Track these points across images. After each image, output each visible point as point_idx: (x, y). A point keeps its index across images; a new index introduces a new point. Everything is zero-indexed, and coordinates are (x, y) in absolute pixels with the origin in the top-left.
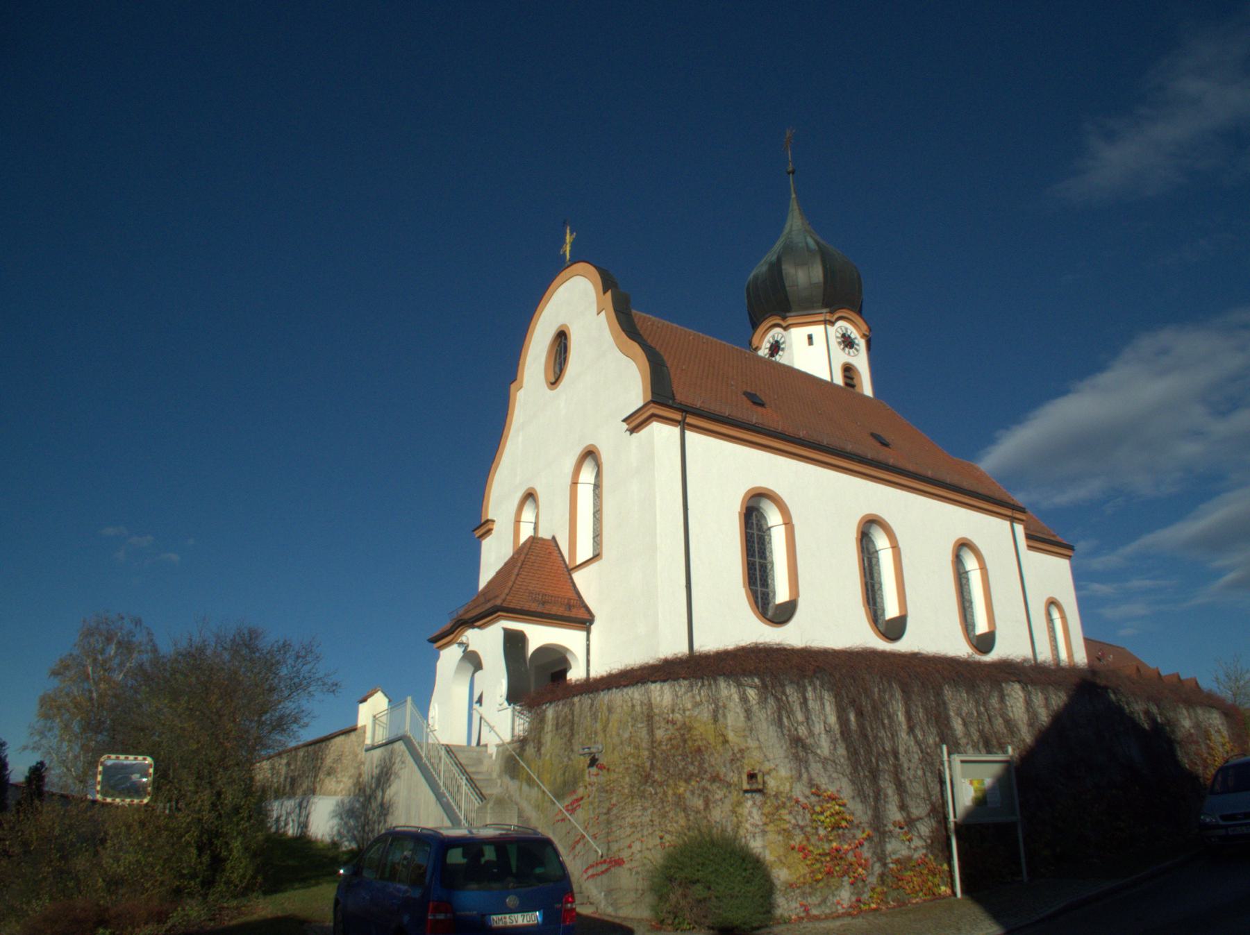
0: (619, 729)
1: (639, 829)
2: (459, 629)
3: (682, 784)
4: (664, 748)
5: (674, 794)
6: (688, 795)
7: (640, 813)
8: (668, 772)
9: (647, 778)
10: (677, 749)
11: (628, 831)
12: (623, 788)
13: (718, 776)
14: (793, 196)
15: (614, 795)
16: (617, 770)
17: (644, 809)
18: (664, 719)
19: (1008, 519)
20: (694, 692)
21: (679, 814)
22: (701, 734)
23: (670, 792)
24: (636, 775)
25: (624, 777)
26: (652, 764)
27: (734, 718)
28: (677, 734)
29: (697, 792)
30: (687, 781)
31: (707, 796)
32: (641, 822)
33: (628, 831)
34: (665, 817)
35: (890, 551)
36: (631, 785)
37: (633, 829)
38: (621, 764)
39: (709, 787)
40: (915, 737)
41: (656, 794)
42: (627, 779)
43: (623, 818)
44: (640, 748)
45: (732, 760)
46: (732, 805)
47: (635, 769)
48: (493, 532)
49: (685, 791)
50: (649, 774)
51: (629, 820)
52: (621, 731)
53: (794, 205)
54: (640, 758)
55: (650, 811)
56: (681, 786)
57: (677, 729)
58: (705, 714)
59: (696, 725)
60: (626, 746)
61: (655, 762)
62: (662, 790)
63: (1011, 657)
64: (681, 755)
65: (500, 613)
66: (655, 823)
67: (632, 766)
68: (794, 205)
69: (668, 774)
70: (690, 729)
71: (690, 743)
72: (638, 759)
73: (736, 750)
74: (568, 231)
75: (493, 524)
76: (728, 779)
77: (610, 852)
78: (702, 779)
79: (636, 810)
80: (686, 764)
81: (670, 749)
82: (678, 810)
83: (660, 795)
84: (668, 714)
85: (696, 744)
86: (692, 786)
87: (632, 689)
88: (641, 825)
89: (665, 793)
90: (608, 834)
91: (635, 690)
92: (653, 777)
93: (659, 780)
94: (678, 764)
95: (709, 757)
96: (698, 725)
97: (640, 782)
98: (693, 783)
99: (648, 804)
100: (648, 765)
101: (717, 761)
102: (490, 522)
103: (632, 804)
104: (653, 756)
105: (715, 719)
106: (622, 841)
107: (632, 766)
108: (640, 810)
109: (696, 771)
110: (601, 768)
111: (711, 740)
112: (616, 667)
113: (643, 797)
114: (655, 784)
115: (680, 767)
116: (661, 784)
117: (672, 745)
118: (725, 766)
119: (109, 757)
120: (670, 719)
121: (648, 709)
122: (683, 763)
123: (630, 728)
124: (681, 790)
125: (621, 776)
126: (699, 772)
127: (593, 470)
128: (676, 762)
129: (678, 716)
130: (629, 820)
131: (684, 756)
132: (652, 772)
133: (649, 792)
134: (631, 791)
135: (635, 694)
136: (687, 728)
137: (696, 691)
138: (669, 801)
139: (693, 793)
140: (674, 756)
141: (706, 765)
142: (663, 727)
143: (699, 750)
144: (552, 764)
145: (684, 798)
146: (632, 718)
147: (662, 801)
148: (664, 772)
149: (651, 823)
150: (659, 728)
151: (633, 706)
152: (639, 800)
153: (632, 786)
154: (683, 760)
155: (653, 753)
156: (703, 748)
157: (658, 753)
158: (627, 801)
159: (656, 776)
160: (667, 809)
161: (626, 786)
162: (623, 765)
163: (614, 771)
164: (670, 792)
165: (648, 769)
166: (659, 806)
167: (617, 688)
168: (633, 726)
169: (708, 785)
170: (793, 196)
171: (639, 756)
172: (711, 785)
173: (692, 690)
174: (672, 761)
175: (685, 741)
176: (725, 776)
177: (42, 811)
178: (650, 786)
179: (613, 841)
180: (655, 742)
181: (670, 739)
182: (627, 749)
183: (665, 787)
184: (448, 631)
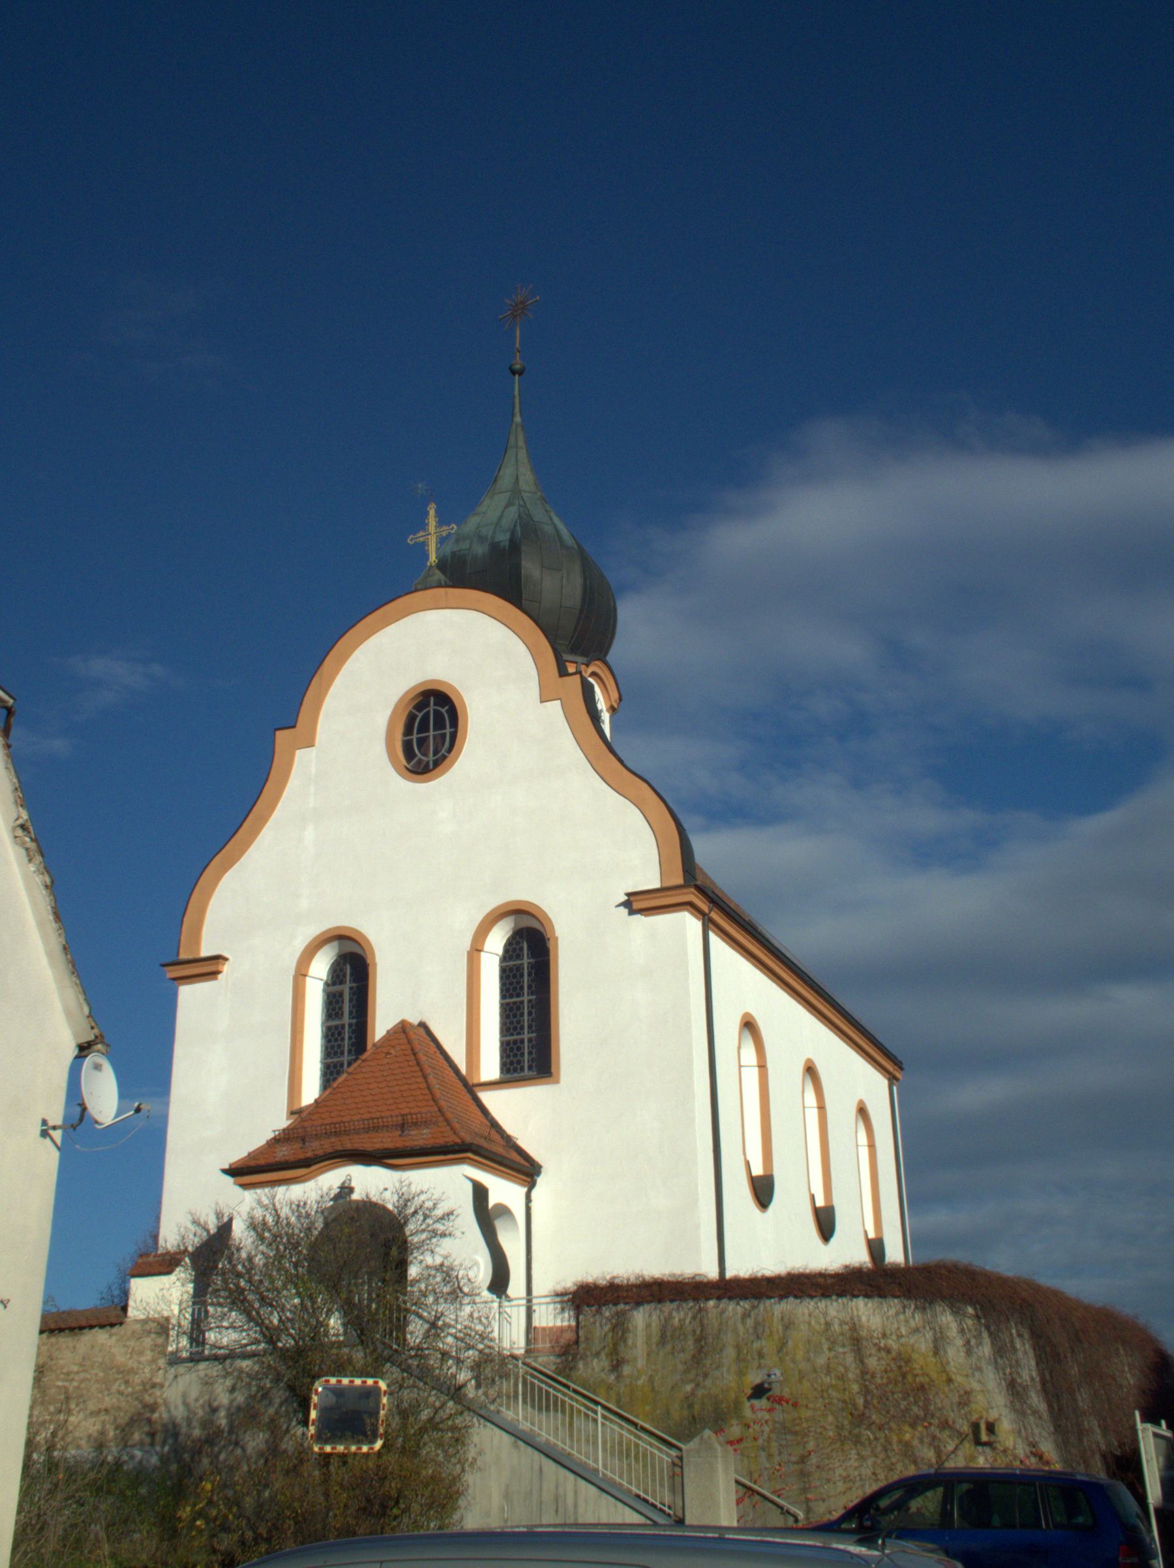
0: (808, 1351)
1: (858, 1484)
2: (328, 1162)
3: (907, 1428)
4: (879, 1381)
5: (900, 1441)
6: (916, 1442)
7: (856, 1464)
8: (888, 1412)
9: (859, 1419)
10: (896, 1384)
11: (841, 1486)
12: (825, 1428)
13: (947, 1422)
14: (518, 419)
15: (811, 1438)
16: (811, 1405)
17: (862, 1458)
18: (876, 1345)
19: (887, 1075)
20: (907, 1314)
21: (909, 1467)
22: (922, 1368)
23: (895, 1439)
24: (844, 1414)
25: (824, 1416)
26: (866, 1401)
27: (955, 1354)
28: (893, 1366)
29: (926, 1440)
30: (913, 1426)
31: (938, 1446)
32: (860, 1475)
33: (841, 1486)
34: (892, 1470)
35: (816, 1111)
36: (837, 1427)
37: (850, 1484)
38: (816, 1398)
39: (938, 1435)
40: (288, 1427)
41: (876, 1439)
42: (830, 1418)
43: (830, 1469)
44: (845, 1379)
45: (960, 1403)
46: (965, 1459)
47: (840, 1405)
48: (220, 976)
49: (913, 1438)
50: (863, 1414)
51: (839, 1471)
52: (812, 1355)
53: (519, 439)
54: (847, 1393)
55: (870, 1461)
56: (906, 1432)
57: (893, 1359)
58: (923, 1343)
59: (915, 1356)
60: (822, 1375)
61: (869, 1398)
62: (883, 1435)
63: (590, 1280)
64: (901, 1392)
65: (470, 1155)
66: (879, 1476)
67: (835, 1401)
68: (519, 439)
69: (888, 1416)
70: (908, 1361)
71: (909, 1377)
72: (844, 1394)
73: (962, 1392)
74: (432, 513)
75: (224, 964)
76: (958, 1426)
77: (811, 1515)
78: (930, 1424)
79: (850, 1458)
80: (908, 1404)
81: (887, 1384)
82: (907, 1461)
83: (882, 1441)
84: (878, 1338)
85: (918, 1379)
86: (919, 1432)
87: (823, 1302)
88: (861, 1479)
89: (887, 1439)
90: (804, 1490)
91: (829, 1304)
92: (869, 1417)
93: (878, 1421)
94: (899, 1404)
95: (934, 1397)
96: (917, 1356)
97: (851, 1423)
98: (920, 1429)
99: (866, 1452)
100: (860, 1401)
101: (943, 1401)
102: (221, 961)
103: (842, 1450)
104: (866, 1391)
105: (936, 1352)
106: (832, 1499)
107: (835, 1401)
108: (856, 1460)
109: (921, 1413)
110: (780, 1400)
111: (934, 1375)
112: (772, 1268)
113: (857, 1441)
114: (873, 1427)
115: (902, 1407)
116: (880, 1428)
117: (888, 1378)
118: (953, 1411)
119: (412, 1333)
120: (882, 1345)
121: (850, 1329)
122: (905, 1403)
123: (827, 1352)
124: (907, 1437)
125: (819, 1413)
126: (925, 1415)
127: (507, 933)
128: (897, 1401)
129: (892, 1343)
130: (839, 1471)
131: (906, 1395)
132: (867, 1412)
133: (865, 1437)
134: (840, 1435)
135: (834, 1309)
136: (903, 1360)
137: (908, 1312)
138: (894, 1450)
139: (921, 1441)
140: (893, 1393)
141: (932, 1407)
142: (875, 1356)
143: (922, 1388)
144: (653, 1390)
145: (912, 1447)
146: (827, 1339)
147: (885, 1449)
148: (884, 1412)
149: (874, 1477)
150: (870, 1355)
151: (828, 1324)
152: (853, 1446)
153: (840, 1428)
154: (904, 1399)
155: (866, 1387)
156: (927, 1386)
157: (872, 1387)
158: (834, 1446)
159: (874, 1417)
160: (893, 1460)
161: (829, 1427)
162: (821, 1400)
163: (806, 1406)
164: (895, 1439)
165: (861, 1407)
166: (882, 1456)
167: (796, 1297)
168: (830, 1349)
169: (937, 1432)
170: (518, 419)
171: (845, 1390)
172: (940, 1432)
173: (904, 1312)
174: (891, 1398)
175: (904, 1376)
176: (954, 1423)
177: (932, 1381)
178: (866, 1429)
179: (816, 1500)
180: (867, 1373)
181: (886, 1371)
182: (824, 1379)
183: (887, 1432)
184: (292, 1163)
